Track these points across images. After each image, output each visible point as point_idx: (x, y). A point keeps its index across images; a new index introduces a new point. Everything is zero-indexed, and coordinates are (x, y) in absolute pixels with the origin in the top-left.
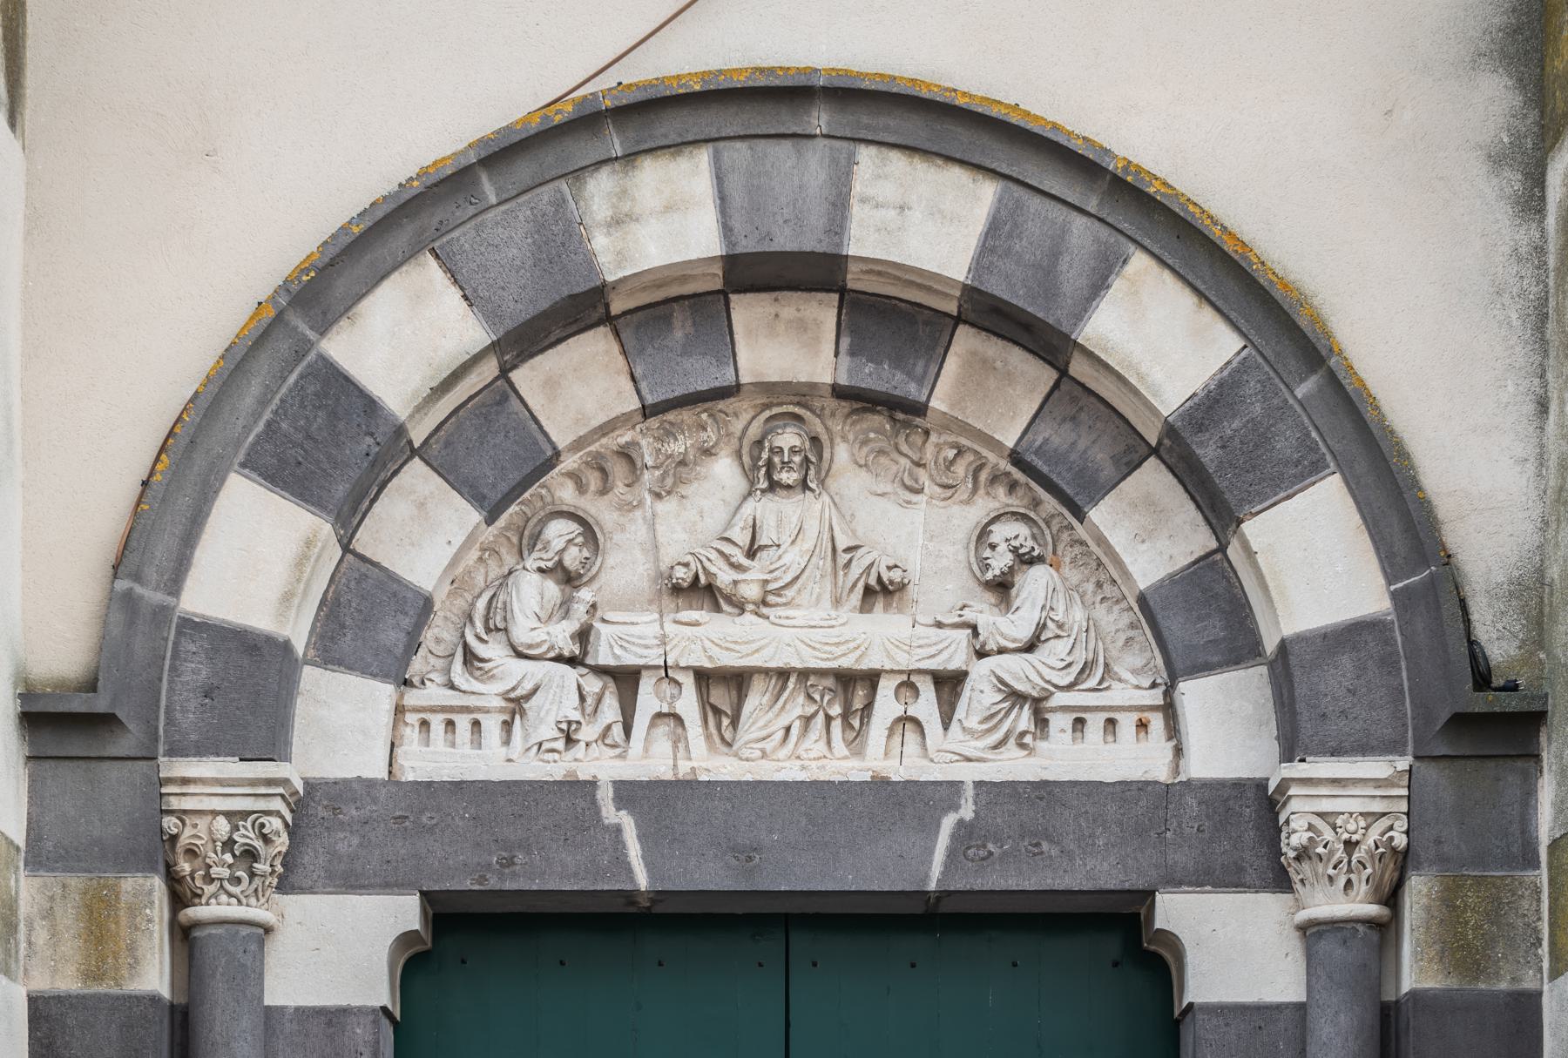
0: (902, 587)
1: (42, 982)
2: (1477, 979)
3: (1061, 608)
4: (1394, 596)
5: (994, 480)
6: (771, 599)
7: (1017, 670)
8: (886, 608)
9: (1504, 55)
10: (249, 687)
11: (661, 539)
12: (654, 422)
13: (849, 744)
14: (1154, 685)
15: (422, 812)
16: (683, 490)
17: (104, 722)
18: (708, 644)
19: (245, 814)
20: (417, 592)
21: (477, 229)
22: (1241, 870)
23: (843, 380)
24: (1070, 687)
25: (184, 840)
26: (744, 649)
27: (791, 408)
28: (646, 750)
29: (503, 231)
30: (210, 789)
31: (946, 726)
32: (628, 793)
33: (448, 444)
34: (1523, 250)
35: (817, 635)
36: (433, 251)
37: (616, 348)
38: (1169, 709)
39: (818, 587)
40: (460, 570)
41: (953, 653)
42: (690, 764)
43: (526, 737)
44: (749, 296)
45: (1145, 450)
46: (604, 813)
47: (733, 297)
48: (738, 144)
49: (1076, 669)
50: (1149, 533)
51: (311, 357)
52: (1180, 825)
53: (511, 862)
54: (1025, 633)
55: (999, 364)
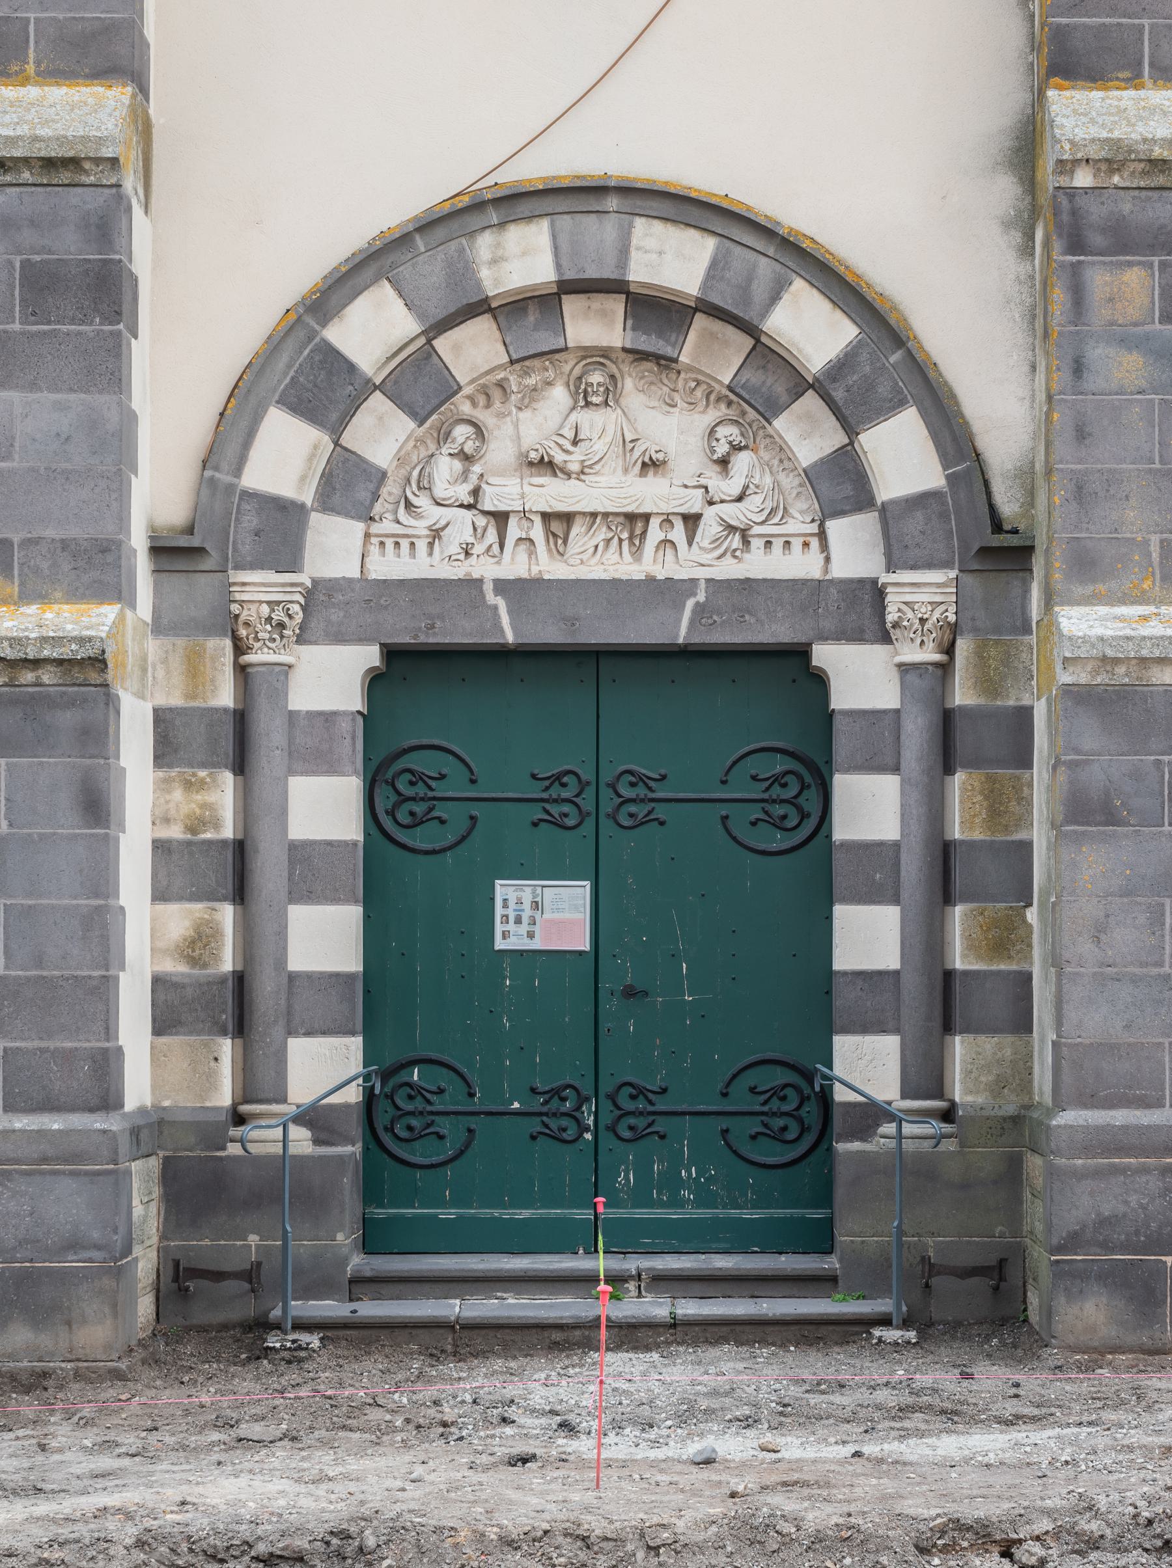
0: (665, 462)
1: (162, 701)
2: (996, 699)
3: (758, 476)
4: (948, 477)
5: (718, 400)
6: (587, 470)
7: (734, 513)
8: (655, 474)
9: (1011, 164)
10: (279, 530)
11: (522, 434)
12: (517, 367)
13: (632, 554)
14: (813, 521)
15: (381, 597)
16: (535, 405)
17: (198, 552)
18: (549, 498)
19: (278, 603)
20: (378, 469)
21: (413, 266)
22: (862, 631)
23: (628, 345)
24: (763, 523)
25: (242, 618)
26: (571, 501)
27: (598, 359)
28: (513, 559)
29: (428, 267)
30: (258, 589)
31: (690, 543)
32: (501, 586)
33: (396, 382)
34: (1022, 278)
35: (613, 492)
36: (388, 279)
37: (495, 326)
38: (822, 535)
39: (614, 463)
40: (403, 453)
41: (694, 502)
42: (538, 568)
43: (442, 552)
44: (573, 296)
45: (807, 386)
46: (487, 598)
47: (563, 297)
48: (565, 216)
49: (766, 512)
50: (807, 434)
51: (317, 340)
52: (826, 604)
53: (433, 627)
54: (736, 491)
55: (720, 335)
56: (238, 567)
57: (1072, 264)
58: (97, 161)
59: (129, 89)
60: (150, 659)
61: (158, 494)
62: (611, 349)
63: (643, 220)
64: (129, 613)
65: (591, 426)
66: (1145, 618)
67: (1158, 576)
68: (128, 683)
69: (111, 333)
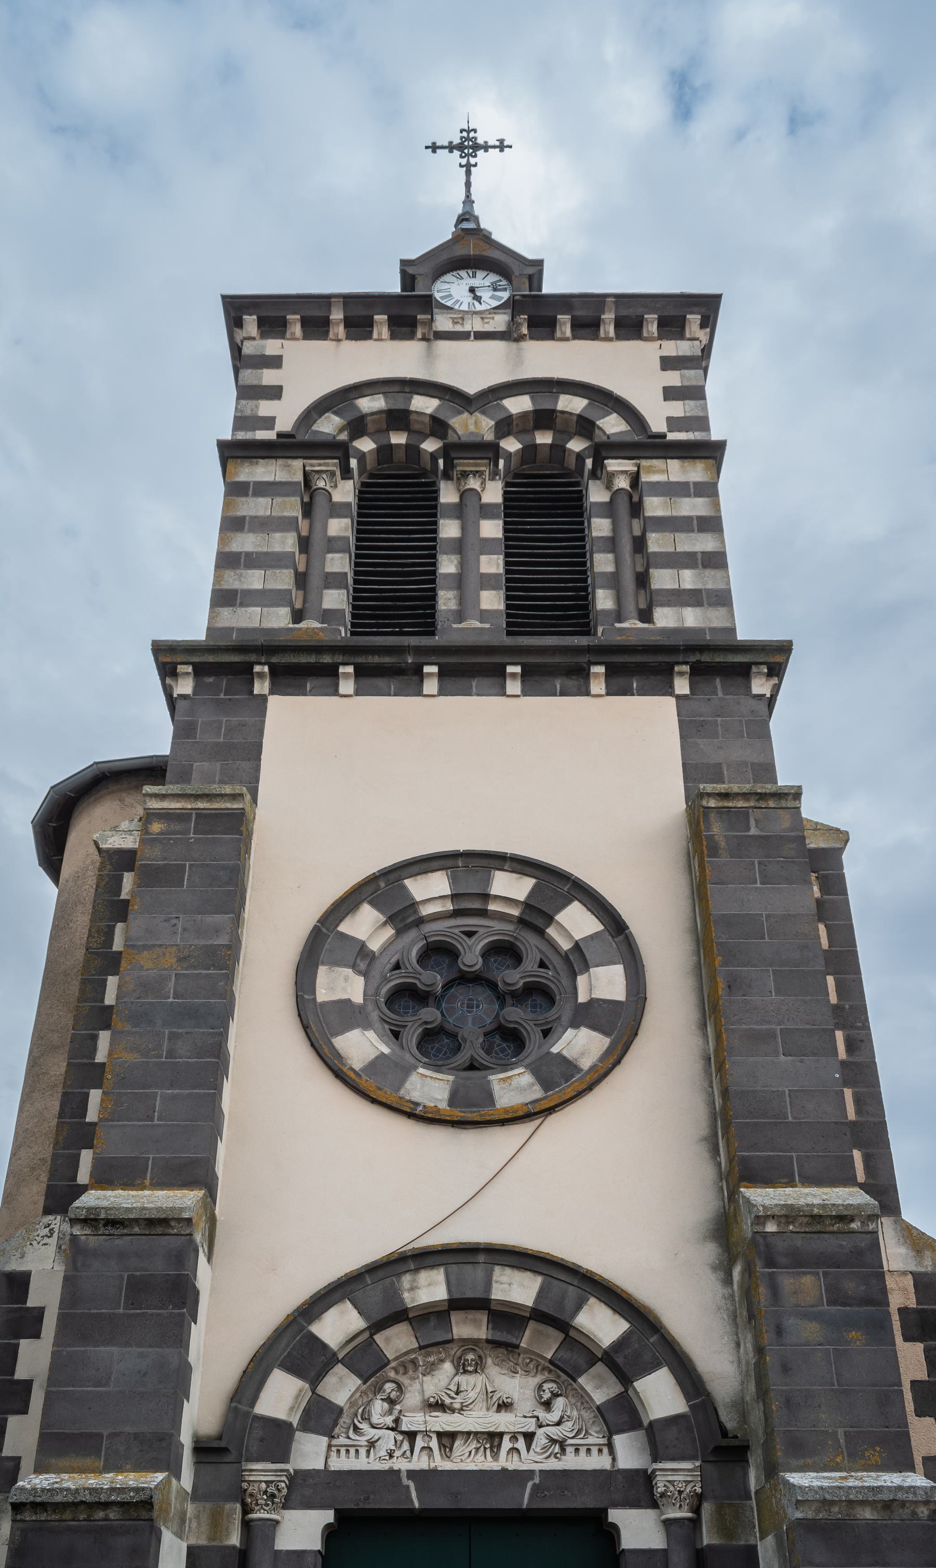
1: (193, 1541)
4: (690, 1406)
7: (554, 1432)
10: (276, 1439)
12: (423, 1351)
13: (492, 1457)
17: (224, 1451)
19: (272, 1482)
23: (490, 1338)
25: (249, 1491)
29: (373, 1292)
30: (260, 1473)
31: (528, 1451)
32: (411, 1474)
35: (481, 1420)
37: (410, 1328)
41: (531, 1426)
43: (375, 1455)
49: (575, 1432)
50: (599, 1388)
53: (368, 1498)
56: (249, 1460)
57: (769, 1273)
58: (180, 1220)
59: (203, 1191)
60: (188, 1515)
61: (200, 1414)
62: (479, 1340)
63: (499, 1267)
64: (174, 1481)
65: (467, 1384)
66: (845, 1478)
67: (845, 1454)
68: (169, 1524)
69: (178, 1314)
